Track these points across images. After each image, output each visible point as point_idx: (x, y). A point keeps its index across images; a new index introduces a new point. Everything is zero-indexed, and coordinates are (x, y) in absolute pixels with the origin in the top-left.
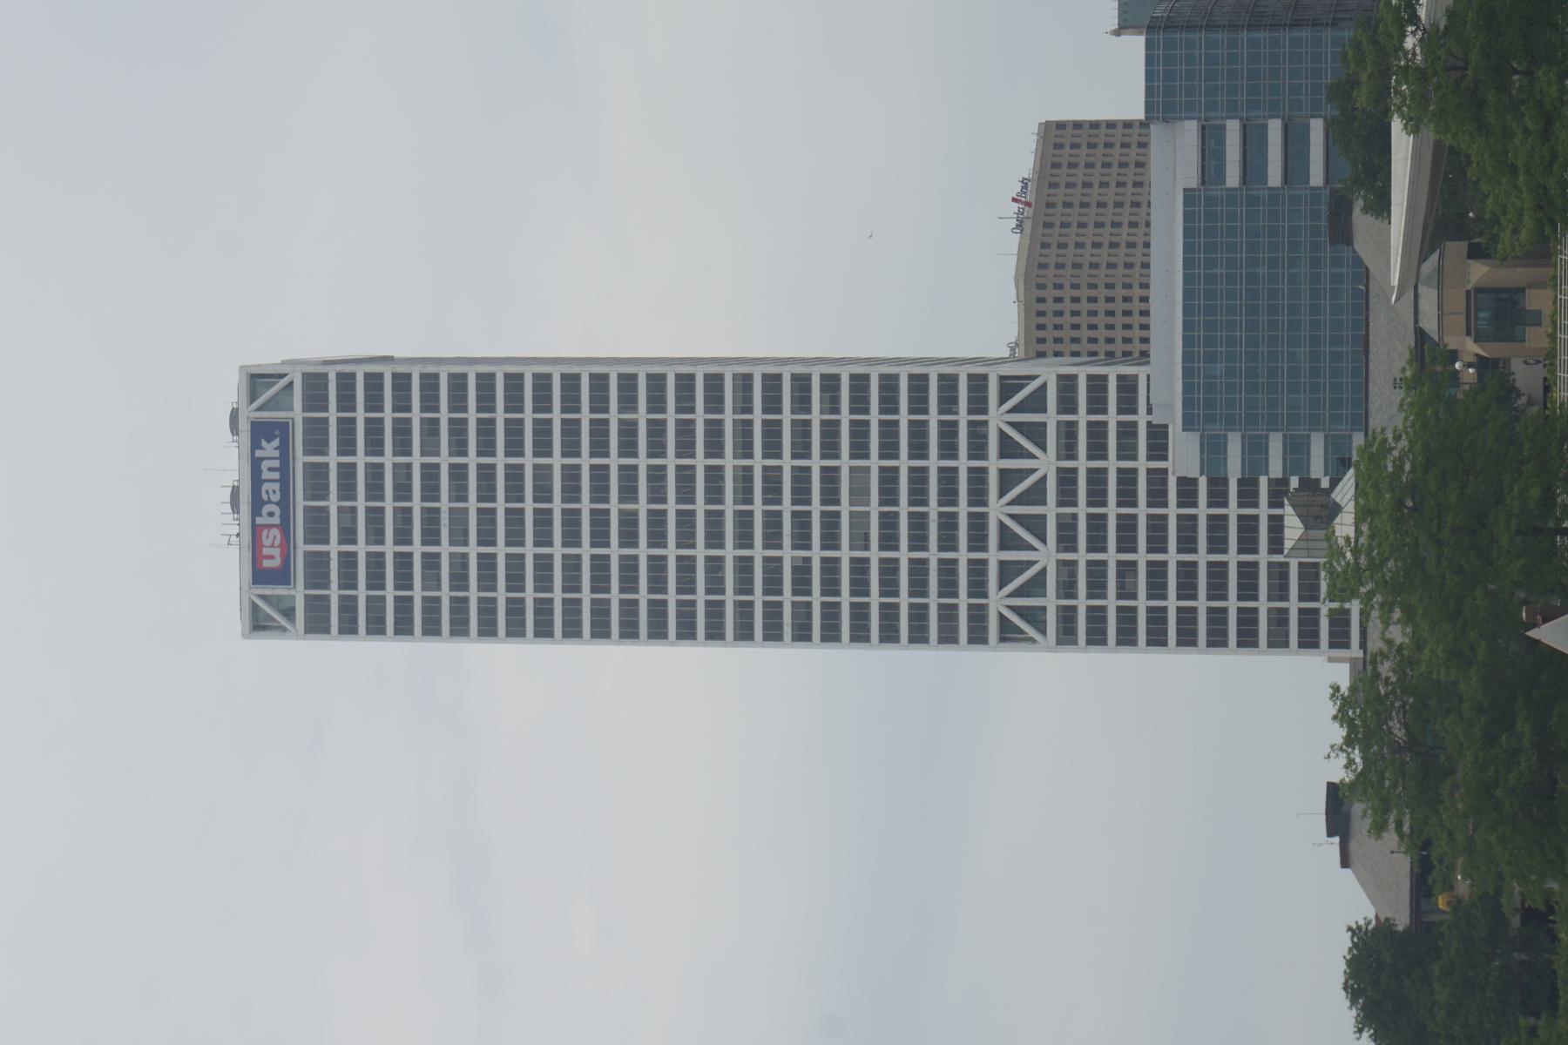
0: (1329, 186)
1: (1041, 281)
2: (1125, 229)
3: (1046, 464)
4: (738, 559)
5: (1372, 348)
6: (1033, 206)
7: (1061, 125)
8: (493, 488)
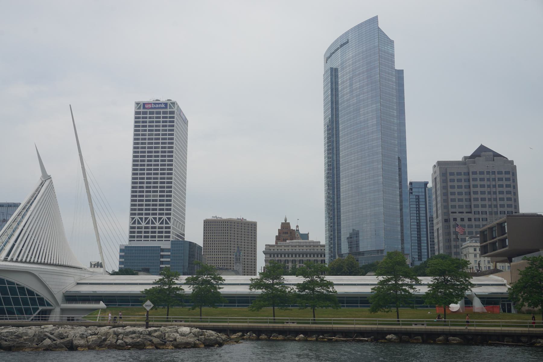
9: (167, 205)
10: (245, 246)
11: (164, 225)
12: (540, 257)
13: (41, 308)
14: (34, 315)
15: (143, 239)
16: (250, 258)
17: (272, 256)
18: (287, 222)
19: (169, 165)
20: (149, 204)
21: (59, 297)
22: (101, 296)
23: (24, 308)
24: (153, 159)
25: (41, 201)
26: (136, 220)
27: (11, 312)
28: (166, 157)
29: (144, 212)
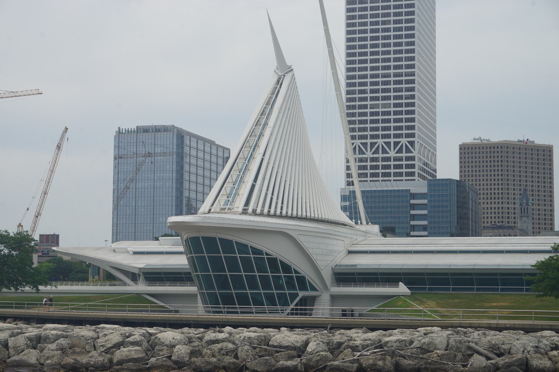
1: (503, 147)
3: (392, 154)
4: (367, 75)
8: (385, 9)
9: (407, 120)
10: (534, 188)
11: (404, 155)
12: (359, 223)
13: (301, 294)
14: (292, 306)
15: (369, 179)
16: (544, 208)
19: (407, 51)
20: (376, 120)
21: (327, 276)
22: (399, 274)
23: (219, 293)
24: (380, 42)
25: (283, 111)
26: (402, 145)
27: (258, 302)
28: (402, 38)
29: (392, 132)
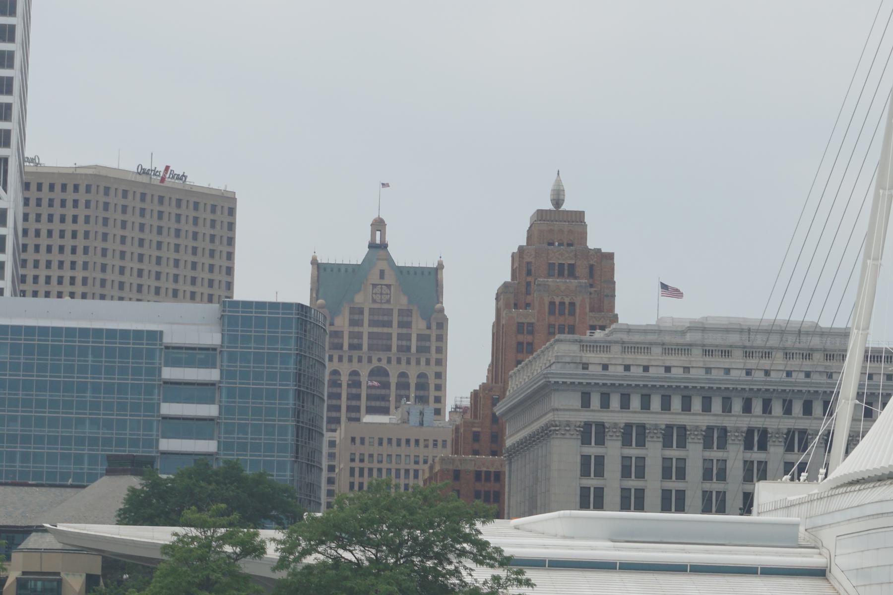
0: (159, 455)
1: (94, 189)
2: (136, 266)
5: (17, 489)
6: (162, 184)
7: (232, 212)
17: (595, 401)
18: (566, 206)
